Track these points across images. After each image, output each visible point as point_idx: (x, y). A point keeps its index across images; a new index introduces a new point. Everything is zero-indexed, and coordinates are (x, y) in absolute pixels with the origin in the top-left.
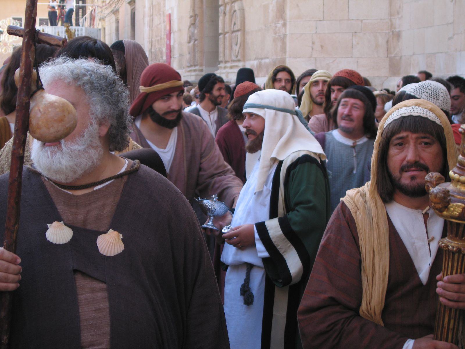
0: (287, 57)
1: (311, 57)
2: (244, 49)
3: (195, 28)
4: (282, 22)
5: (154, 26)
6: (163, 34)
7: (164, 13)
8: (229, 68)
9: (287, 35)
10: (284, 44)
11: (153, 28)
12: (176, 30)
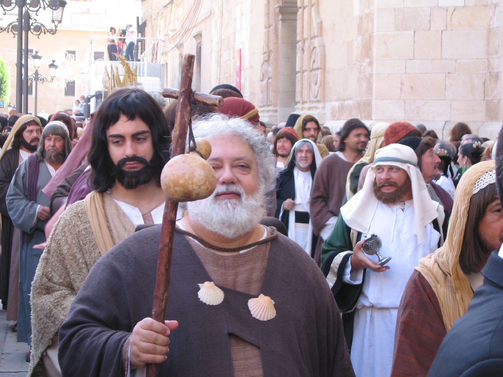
0: (373, 98)
1: (399, 99)
2: (324, 89)
3: (269, 65)
4: (368, 61)
5: (222, 62)
6: (232, 70)
7: (233, 48)
8: (307, 109)
9: (373, 74)
10: (370, 83)
11: (221, 64)
12: (248, 67)
